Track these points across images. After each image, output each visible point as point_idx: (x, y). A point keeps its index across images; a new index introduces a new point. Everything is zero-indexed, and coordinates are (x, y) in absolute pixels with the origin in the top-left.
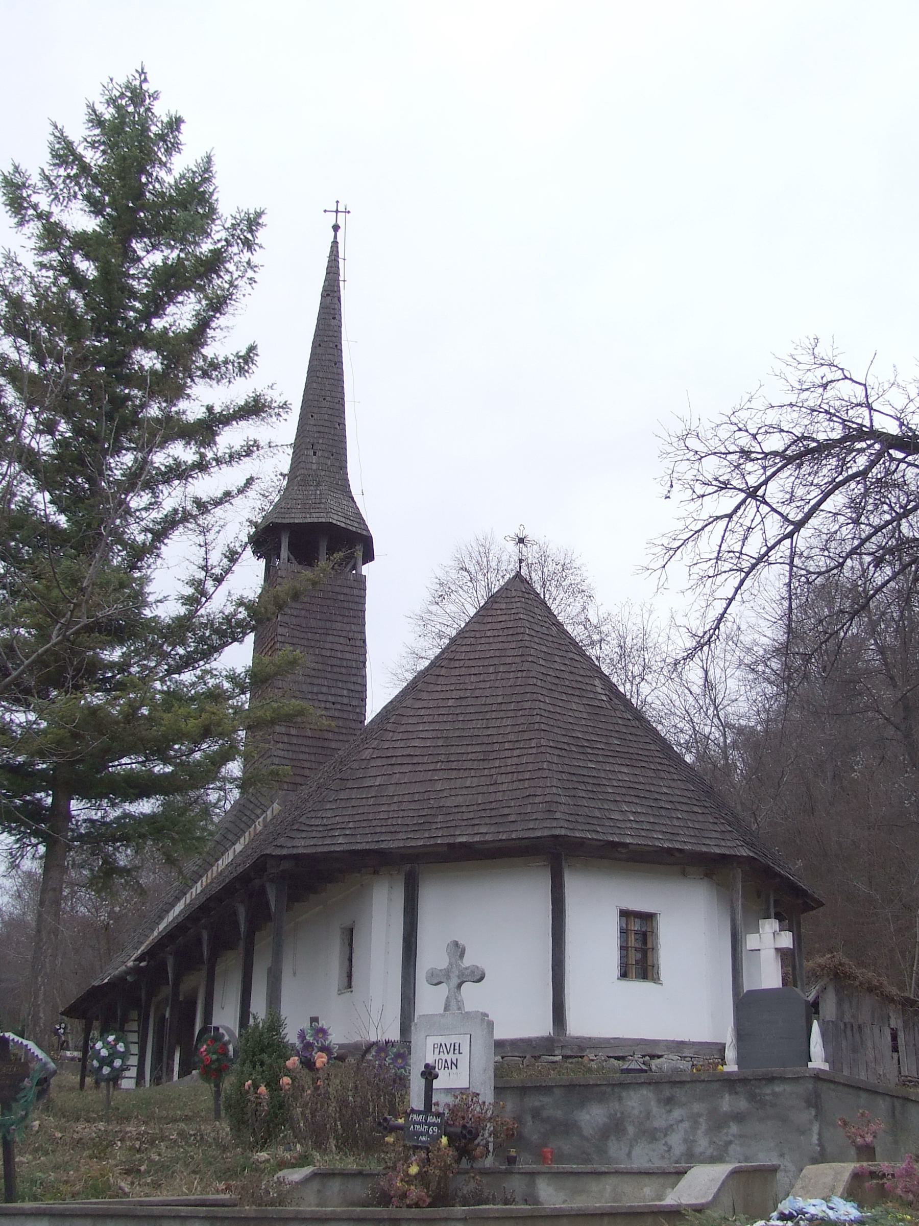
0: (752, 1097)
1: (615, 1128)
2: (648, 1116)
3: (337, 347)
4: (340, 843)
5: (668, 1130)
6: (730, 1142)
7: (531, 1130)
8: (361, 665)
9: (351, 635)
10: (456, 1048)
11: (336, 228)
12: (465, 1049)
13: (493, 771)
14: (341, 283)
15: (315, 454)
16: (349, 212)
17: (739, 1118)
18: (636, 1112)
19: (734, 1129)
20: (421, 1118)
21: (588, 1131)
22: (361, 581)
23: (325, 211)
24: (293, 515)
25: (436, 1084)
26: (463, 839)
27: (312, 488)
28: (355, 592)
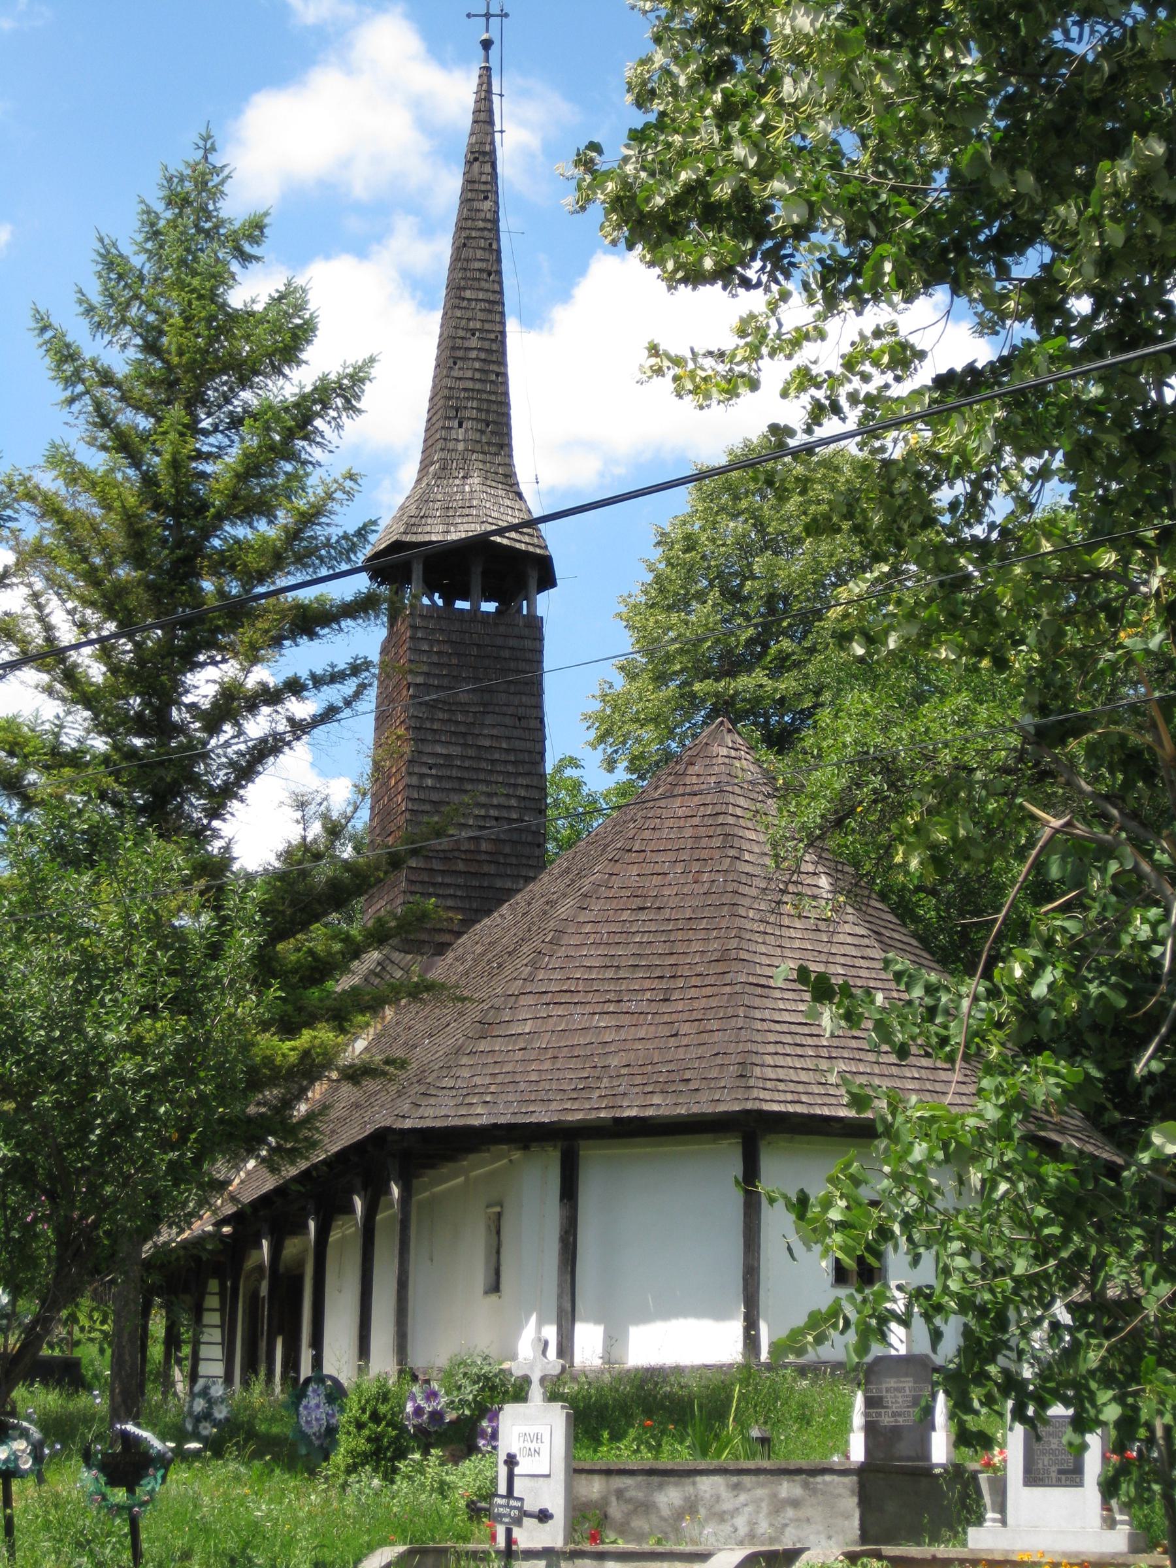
0: (806, 1486)
1: (690, 1508)
2: (718, 1499)
3: (494, 273)
4: (481, 1116)
5: (736, 1511)
6: (786, 1525)
7: (616, 1510)
8: (538, 758)
9: (521, 711)
10: (538, 1438)
11: (487, 44)
12: (546, 1438)
13: (674, 1017)
14: (497, 136)
15: (460, 425)
16: (506, 15)
17: (795, 1503)
18: (708, 1495)
19: (790, 1513)
20: (503, 1501)
21: (666, 1512)
22: (535, 626)
23: (469, 16)
24: (428, 529)
25: (517, 1471)
26: (632, 1113)
27: (457, 482)
28: (528, 644)
